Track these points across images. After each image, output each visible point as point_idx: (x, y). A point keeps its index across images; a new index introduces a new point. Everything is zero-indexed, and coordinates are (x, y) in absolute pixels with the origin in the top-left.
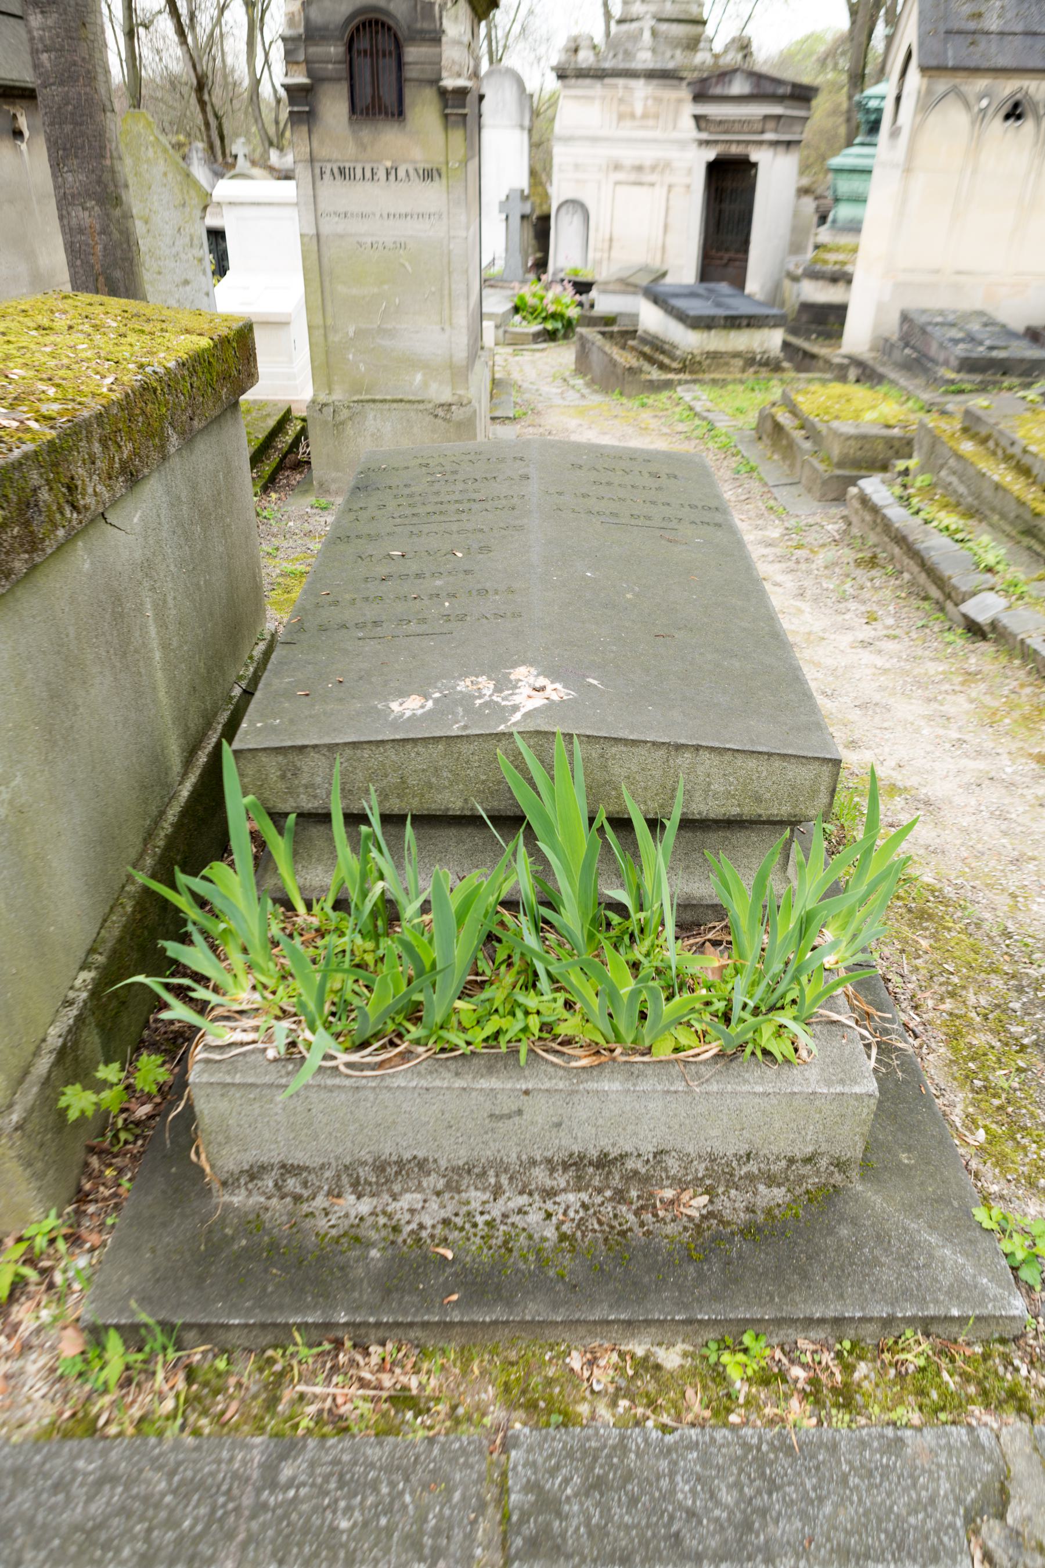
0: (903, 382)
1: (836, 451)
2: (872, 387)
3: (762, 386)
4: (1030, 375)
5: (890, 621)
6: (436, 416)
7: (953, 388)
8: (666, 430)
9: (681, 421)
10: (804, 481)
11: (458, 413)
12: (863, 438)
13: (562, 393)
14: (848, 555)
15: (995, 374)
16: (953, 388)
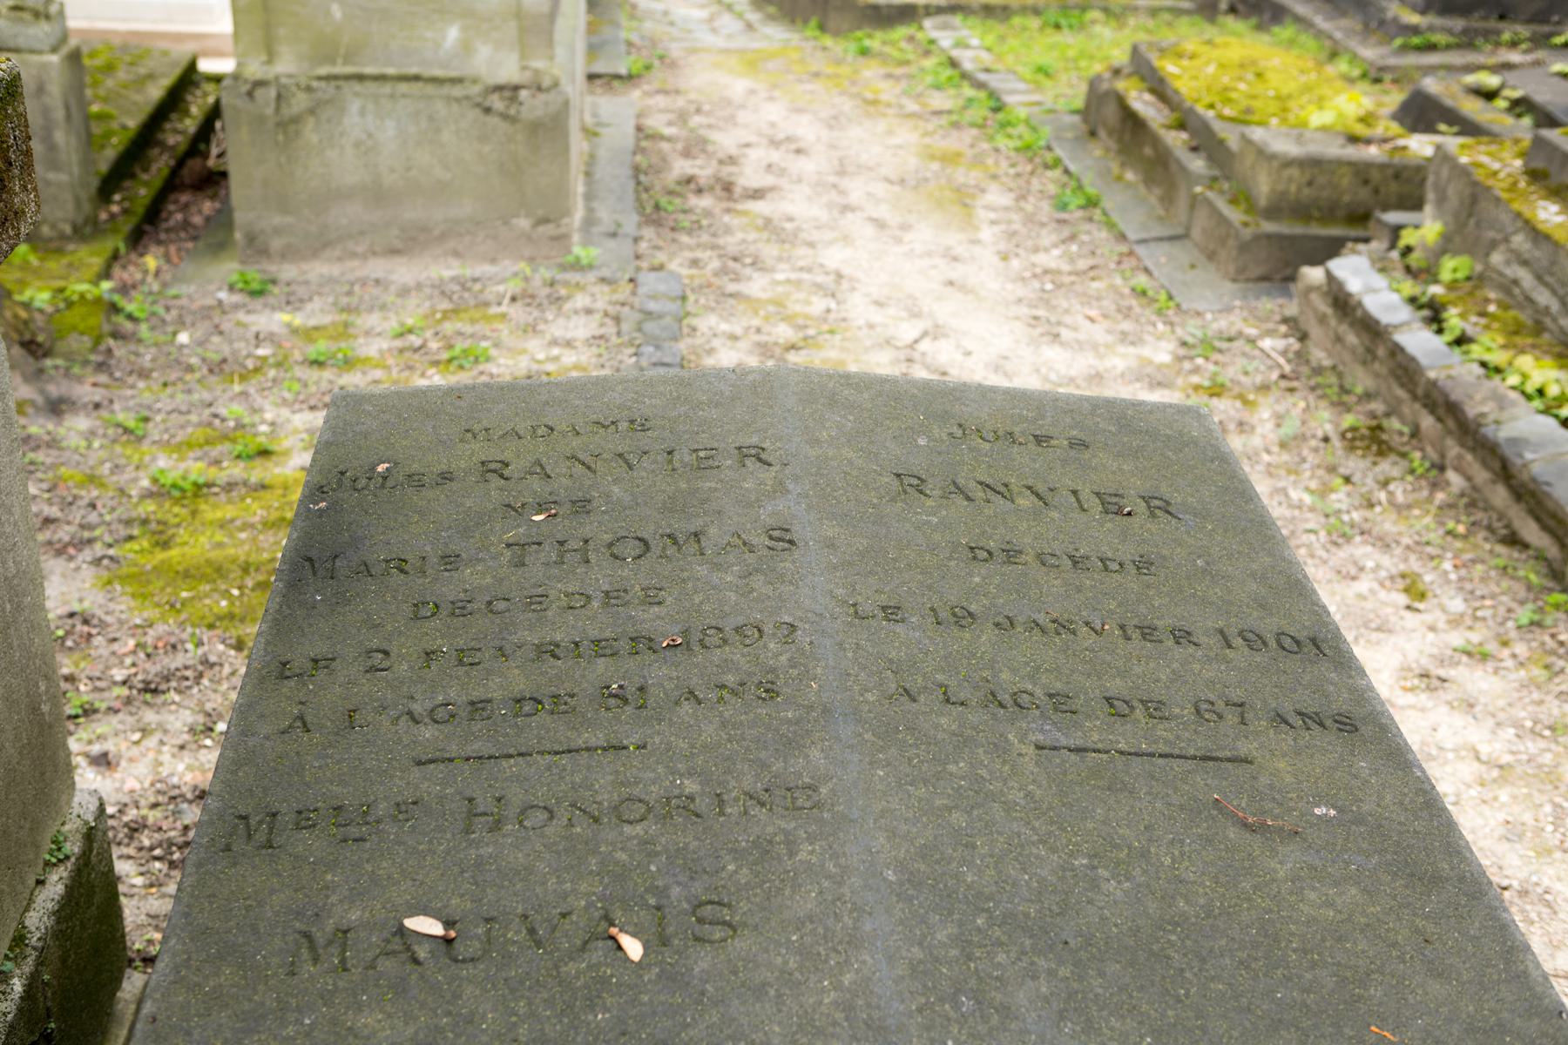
0: (1320, 21)
1: (1263, 186)
2: (1260, 28)
3: (1074, 21)
4: (1545, 21)
5: (1457, 605)
6: (488, 110)
7: (1416, 40)
8: (912, 106)
9: (938, 87)
10: (1196, 233)
11: (532, 106)
12: (1313, 164)
13: (711, 20)
14: (1325, 421)
15: (1485, 18)
16: (1416, 40)
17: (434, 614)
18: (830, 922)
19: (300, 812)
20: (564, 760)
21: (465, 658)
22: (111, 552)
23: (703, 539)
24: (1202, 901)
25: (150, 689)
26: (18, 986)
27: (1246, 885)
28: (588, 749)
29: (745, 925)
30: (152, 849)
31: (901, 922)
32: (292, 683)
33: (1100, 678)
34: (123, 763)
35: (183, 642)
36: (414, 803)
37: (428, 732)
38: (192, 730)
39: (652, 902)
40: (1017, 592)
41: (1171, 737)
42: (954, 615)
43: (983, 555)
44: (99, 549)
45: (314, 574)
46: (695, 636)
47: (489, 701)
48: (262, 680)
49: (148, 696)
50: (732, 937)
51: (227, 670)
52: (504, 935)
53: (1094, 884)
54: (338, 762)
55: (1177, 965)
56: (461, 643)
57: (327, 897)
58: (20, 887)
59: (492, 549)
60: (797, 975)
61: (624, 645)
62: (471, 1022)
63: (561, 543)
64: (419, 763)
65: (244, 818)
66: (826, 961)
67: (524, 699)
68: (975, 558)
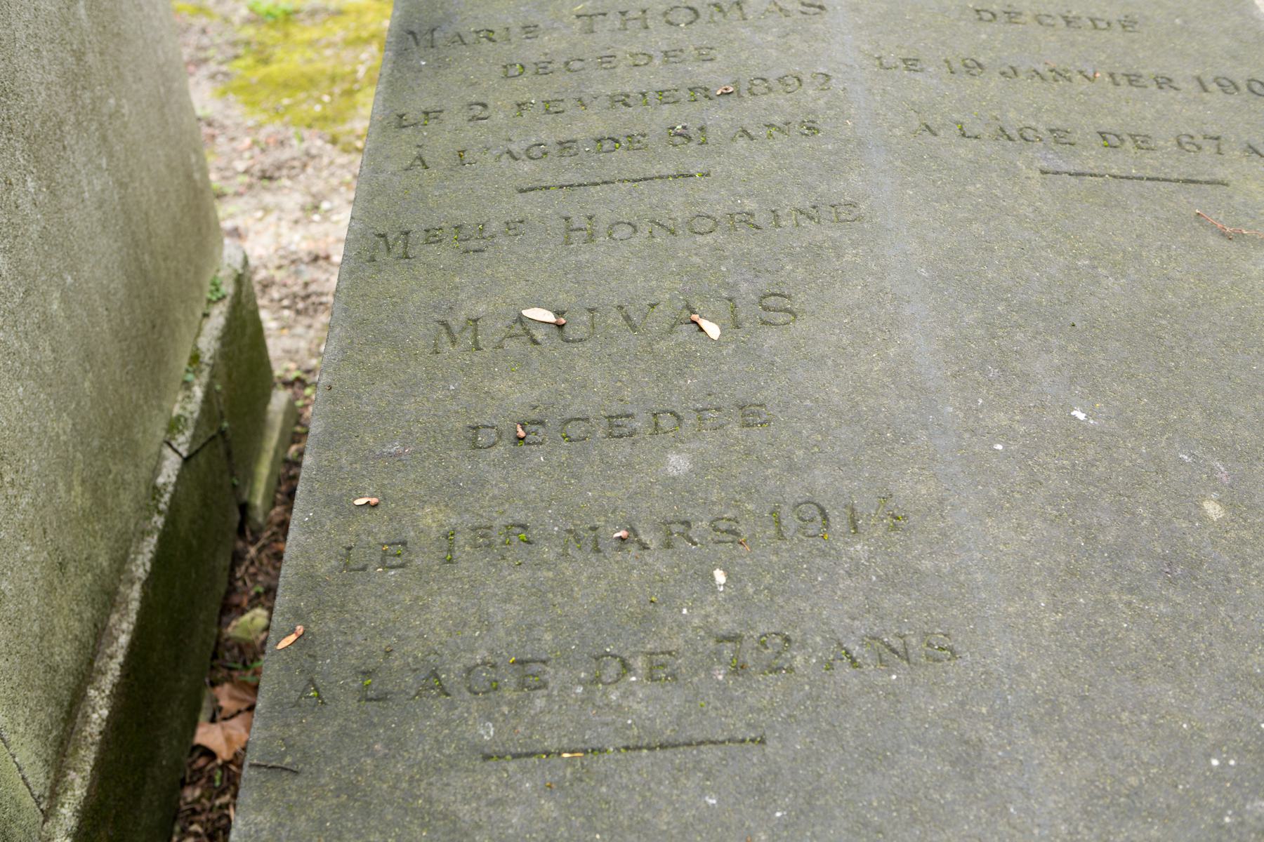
17: (520, 74)
18: (875, 308)
19: (427, 231)
20: (642, 186)
21: (551, 108)
22: (224, 68)
23: (744, 6)
24: (1187, 294)
25: (266, 177)
26: (198, 392)
27: (1225, 282)
28: (661, 177)
29: (804, 311)
30: (281, 300)
31: (935, 309)
32: (410, 130)
33: (1094, 117)
34: (251, 236)
35: (289, 139)
36: (521, 222)
37: (526, 167)
38: (303, 209)
39: (725, 294)
40: (1019, 46)
41: (1158, 165)
42: (966, 66)
43: (988, 16)
44: (213, 67)
45: (417, 44)
46: (744, 86)
47: (574, 141)
48: (384, 129)
49: (266, 183)
50: (794, 321)
51: (325, 160)
52: (605, 322)
53: (1096, 280)
54: (455, 191)
55: (1167, 343)
56: (546, 97)
57: (458, 294)
58: (191, 318)
59: (565, 20)
60: (850, 349)
61: (684, 95)
62: (585, 386)
63: (623, 13)
64: (522, 191)
65: (383, 236)
66: (873, 339)
67: (603, 139)
68: (981, 19)
